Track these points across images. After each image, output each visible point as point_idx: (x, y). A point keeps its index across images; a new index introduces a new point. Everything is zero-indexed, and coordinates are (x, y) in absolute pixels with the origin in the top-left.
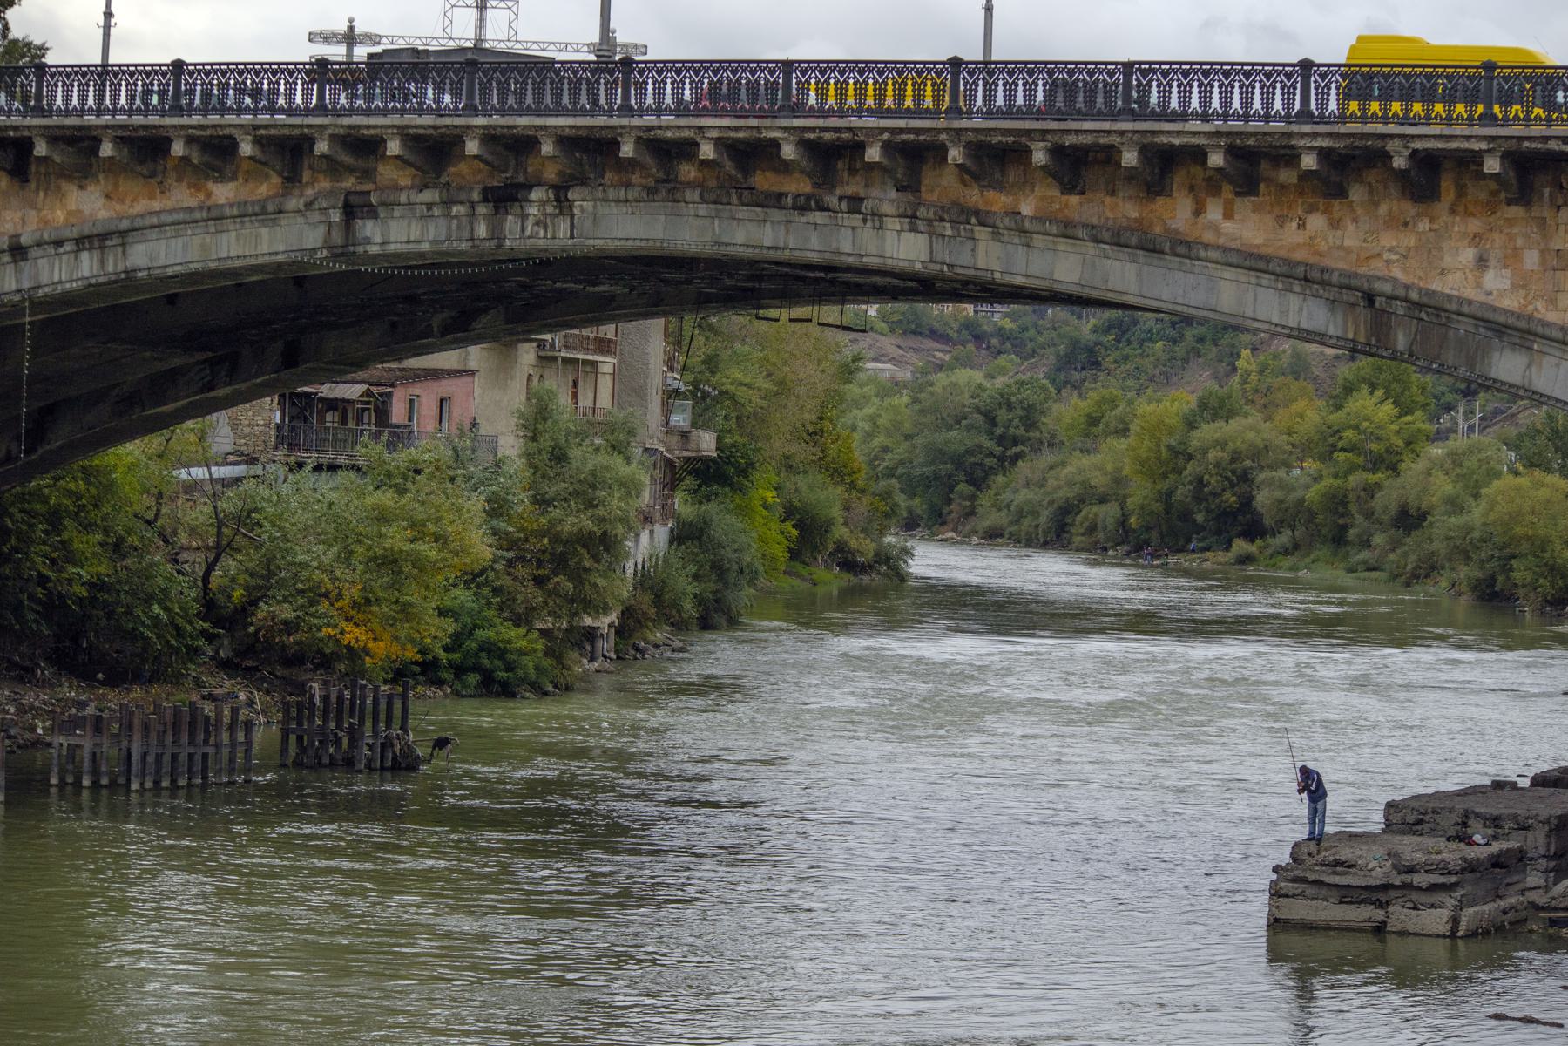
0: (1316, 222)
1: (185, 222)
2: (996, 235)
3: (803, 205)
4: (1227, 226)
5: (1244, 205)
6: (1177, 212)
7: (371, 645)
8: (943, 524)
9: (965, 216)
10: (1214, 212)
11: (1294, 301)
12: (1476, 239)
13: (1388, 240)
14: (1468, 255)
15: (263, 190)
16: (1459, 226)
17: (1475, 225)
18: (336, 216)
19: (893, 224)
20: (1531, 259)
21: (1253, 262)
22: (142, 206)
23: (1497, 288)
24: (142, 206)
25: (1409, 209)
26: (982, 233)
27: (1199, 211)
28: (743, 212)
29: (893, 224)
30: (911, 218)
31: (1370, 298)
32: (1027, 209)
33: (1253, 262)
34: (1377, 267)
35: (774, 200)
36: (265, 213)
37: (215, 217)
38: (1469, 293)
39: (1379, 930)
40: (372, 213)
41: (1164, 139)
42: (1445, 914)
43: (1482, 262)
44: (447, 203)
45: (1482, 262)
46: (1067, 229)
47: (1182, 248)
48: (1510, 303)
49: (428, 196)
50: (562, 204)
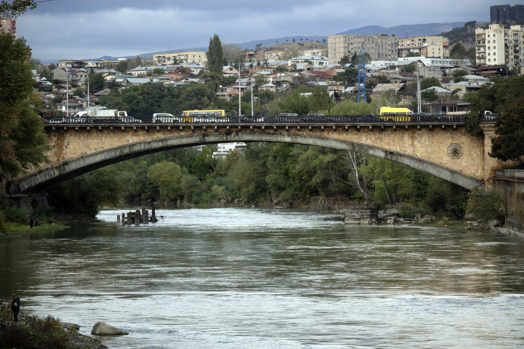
0: (344, 135)
1: (177, 138)
2: (301, 137)
3: (273, 134)
4: (332, 135)
5: (335, 133)
6: (325, 134)
7: (510, 48)
8: (8, 46)
9: (296, 135)
10: (331, 134)
11: (342, 145)
12: (366, 136)
13: (354, 136)
14: (365, 138)
15: (189, 133)
16: (363, 134)
17: (366, 134)
18: (201, 137)
19: (286, 136)
20: (373, 138)
21: (337, 140)
22: (169, 136)
23: (369, 142)
24: (169, 136)
25: (357, 132)
26: (299, 137)
27: (328, 133)
28: (264, 135)
29: (286, 136)
30: (289, 136)
31: (352, 144)
32: (305, 134)
33: (337, 140)
34: (353, 140)
35: (269, 133)
36: (190, 136)
37: (182, 137)
38: (365, 143)
39: (359, 224)
40: (207, 136)
41: (156, 266)
42: (368, 221)
43: (367, 139)
44: (219, 135)
45: (367, 139)
46: (311, 137)
47: (327, 139)
48: (371, 144)
49: (216, 134)
50: (237, 134)
